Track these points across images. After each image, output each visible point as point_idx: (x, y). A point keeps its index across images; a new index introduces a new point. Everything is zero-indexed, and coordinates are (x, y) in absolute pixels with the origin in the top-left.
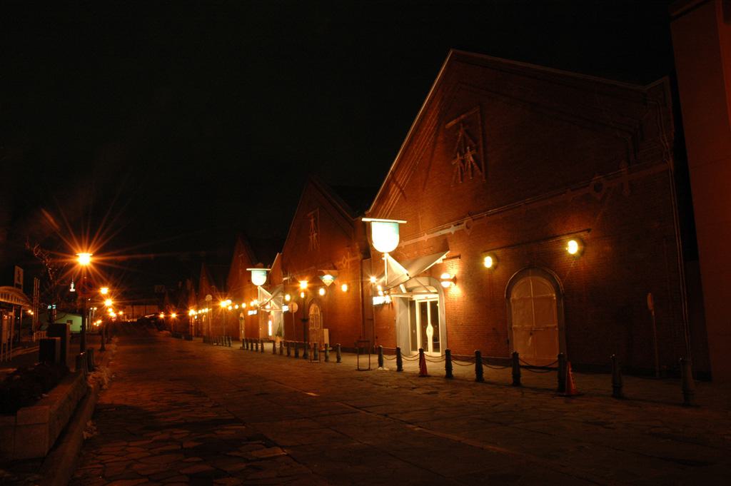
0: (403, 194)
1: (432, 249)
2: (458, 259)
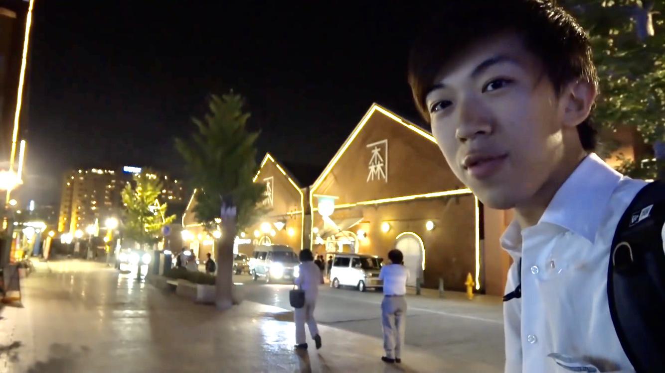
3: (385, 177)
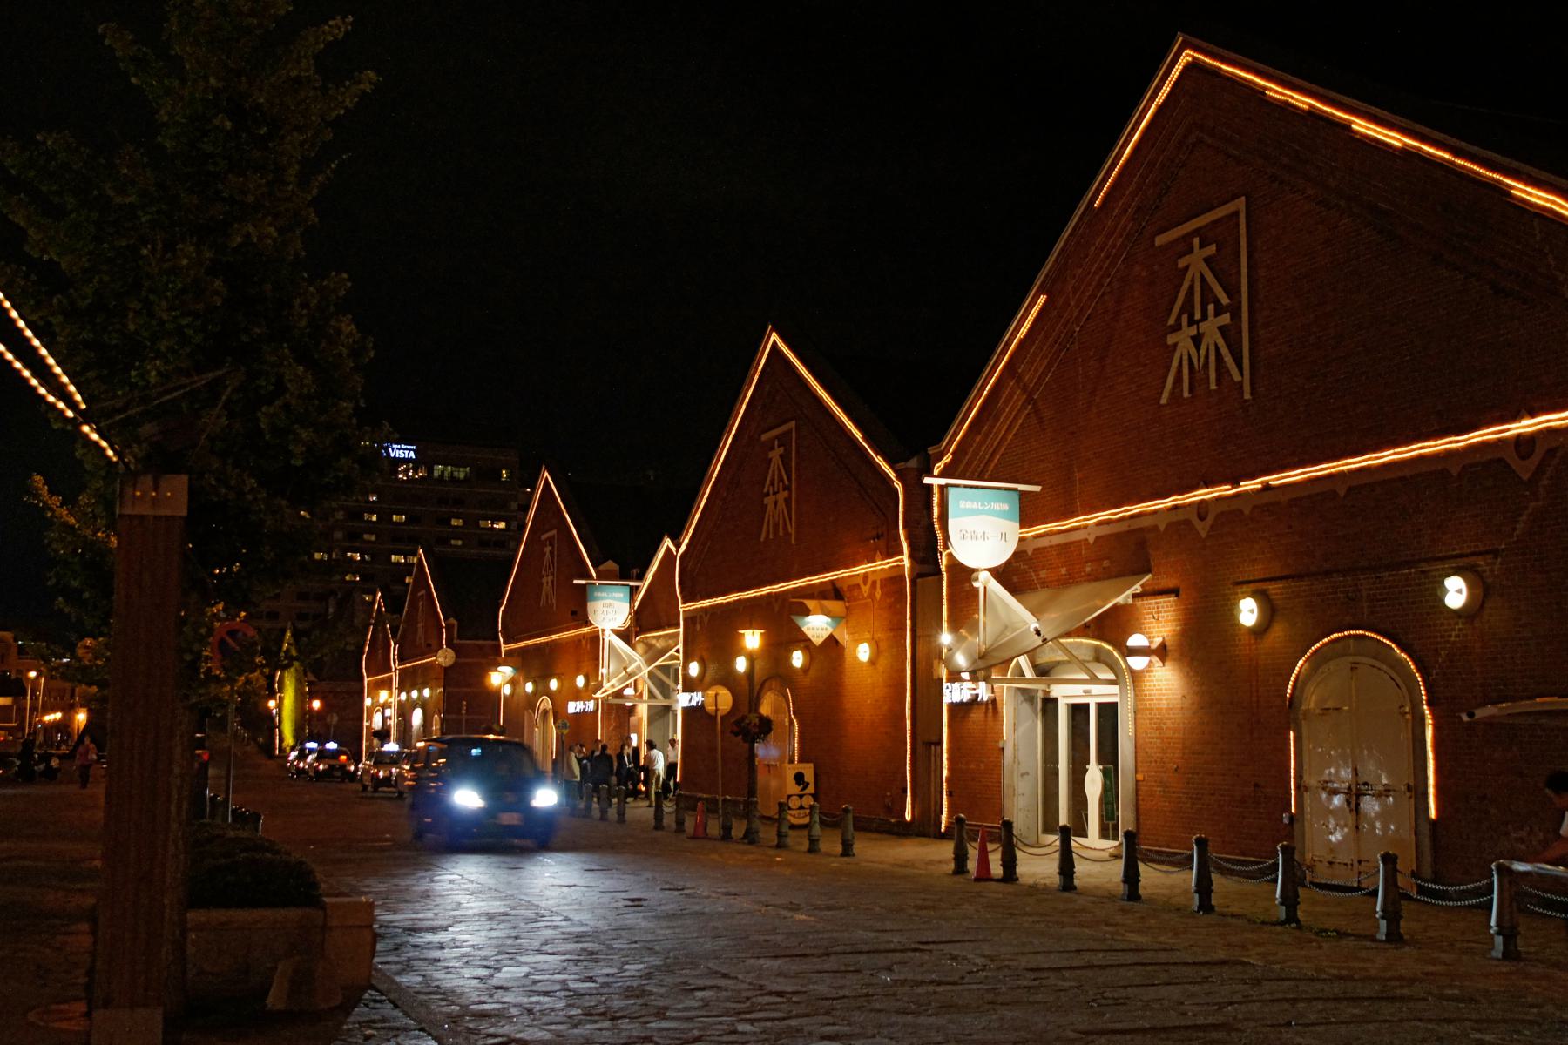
0: (1036, 411)
1: (1106, 563)
2: (1172, 599)
3: (1241, 376)
